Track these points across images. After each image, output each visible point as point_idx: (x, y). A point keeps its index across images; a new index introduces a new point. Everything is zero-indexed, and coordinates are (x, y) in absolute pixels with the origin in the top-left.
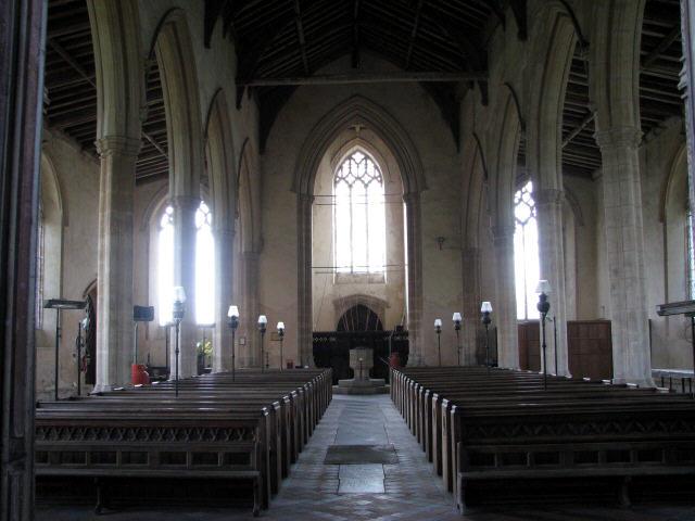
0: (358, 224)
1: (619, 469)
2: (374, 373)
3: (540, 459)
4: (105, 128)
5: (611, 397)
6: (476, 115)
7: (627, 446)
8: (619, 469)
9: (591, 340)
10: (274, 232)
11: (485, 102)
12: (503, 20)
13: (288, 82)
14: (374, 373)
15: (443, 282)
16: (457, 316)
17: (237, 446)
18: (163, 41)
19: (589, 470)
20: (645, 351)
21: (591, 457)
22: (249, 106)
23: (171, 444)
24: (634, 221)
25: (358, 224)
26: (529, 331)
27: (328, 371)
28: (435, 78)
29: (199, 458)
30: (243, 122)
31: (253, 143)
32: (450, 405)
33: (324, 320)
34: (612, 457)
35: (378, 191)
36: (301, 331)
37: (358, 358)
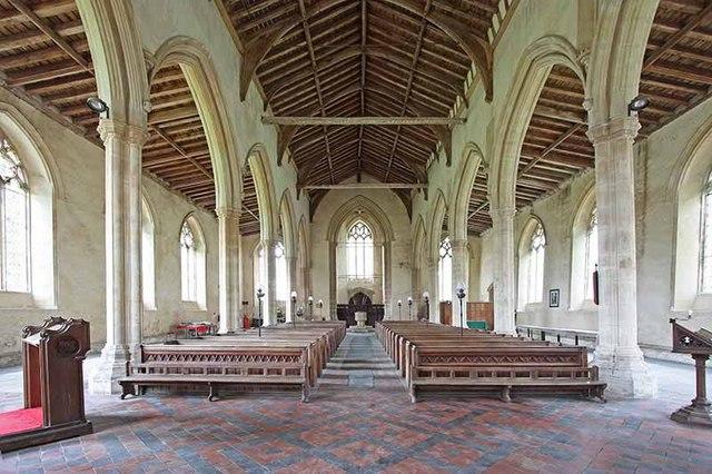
0: (358, 259)
1: (504, 381)
2: (367, 323)
3: (458, 374)
4: (221, 202)
5: (371, 362)
6: (423, 207)
7: (510, 369)
8: (504, 381)
9: (483, 314)
10: (314, 262)
11: (426, 199)
12: (437, 157)
13: (323, 187)
14: (367, 323)
15: (401, 280)
16: (410, 299)
17: (292, 365)
18: (252, 161)
19: (486, 381)
20: (586, 278)
21: (489, 374)
22: (304, 198)
23: (275, 364)
24: (509, 255)
25: (358, 259)
26: (445, 306)
27: (345, 322)
28: (401, 186)
29: (289, 372)
30: (301, 206)
31: (307, 217)
32: (411, 346)
33: (342, 299)
34: (500, 375)
35: (369, 241)
36: (331, 304)
37: (359, 316)
